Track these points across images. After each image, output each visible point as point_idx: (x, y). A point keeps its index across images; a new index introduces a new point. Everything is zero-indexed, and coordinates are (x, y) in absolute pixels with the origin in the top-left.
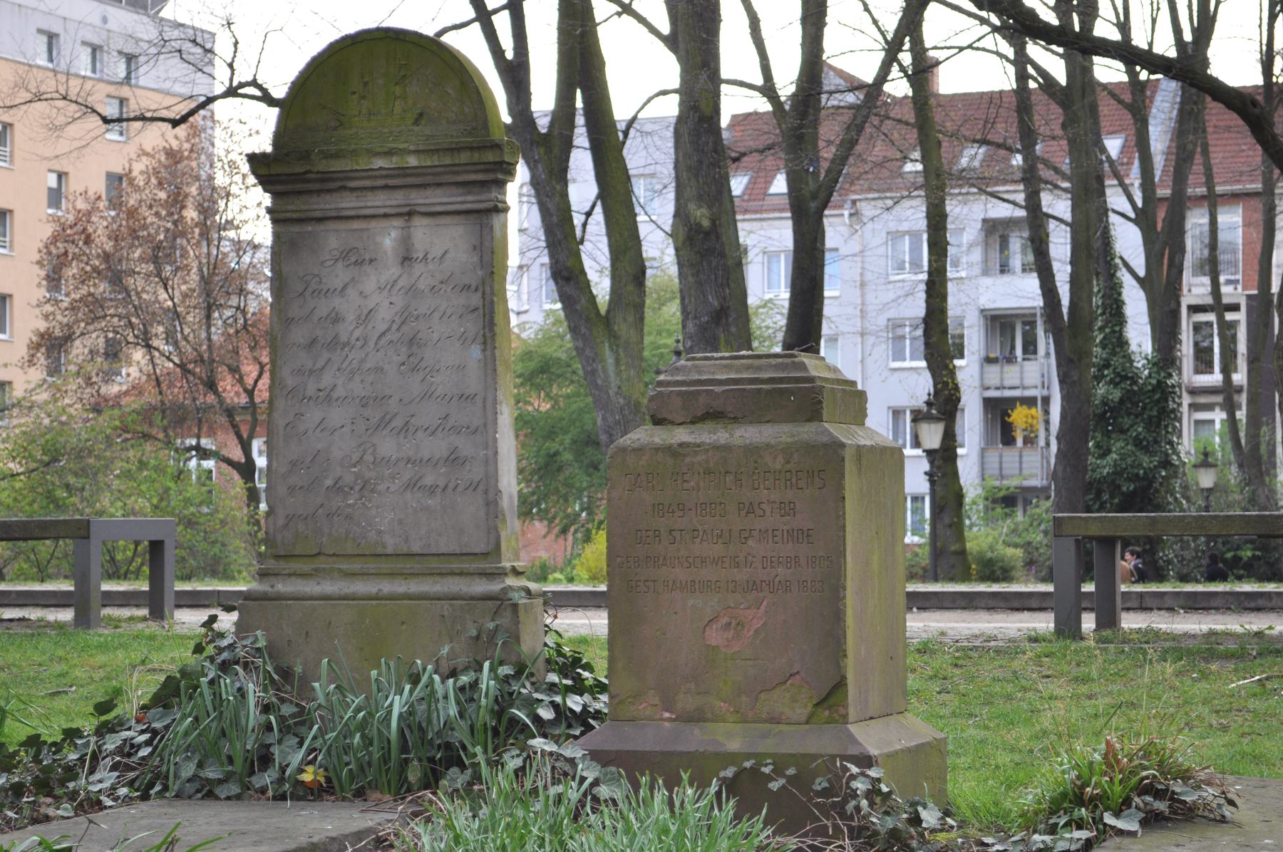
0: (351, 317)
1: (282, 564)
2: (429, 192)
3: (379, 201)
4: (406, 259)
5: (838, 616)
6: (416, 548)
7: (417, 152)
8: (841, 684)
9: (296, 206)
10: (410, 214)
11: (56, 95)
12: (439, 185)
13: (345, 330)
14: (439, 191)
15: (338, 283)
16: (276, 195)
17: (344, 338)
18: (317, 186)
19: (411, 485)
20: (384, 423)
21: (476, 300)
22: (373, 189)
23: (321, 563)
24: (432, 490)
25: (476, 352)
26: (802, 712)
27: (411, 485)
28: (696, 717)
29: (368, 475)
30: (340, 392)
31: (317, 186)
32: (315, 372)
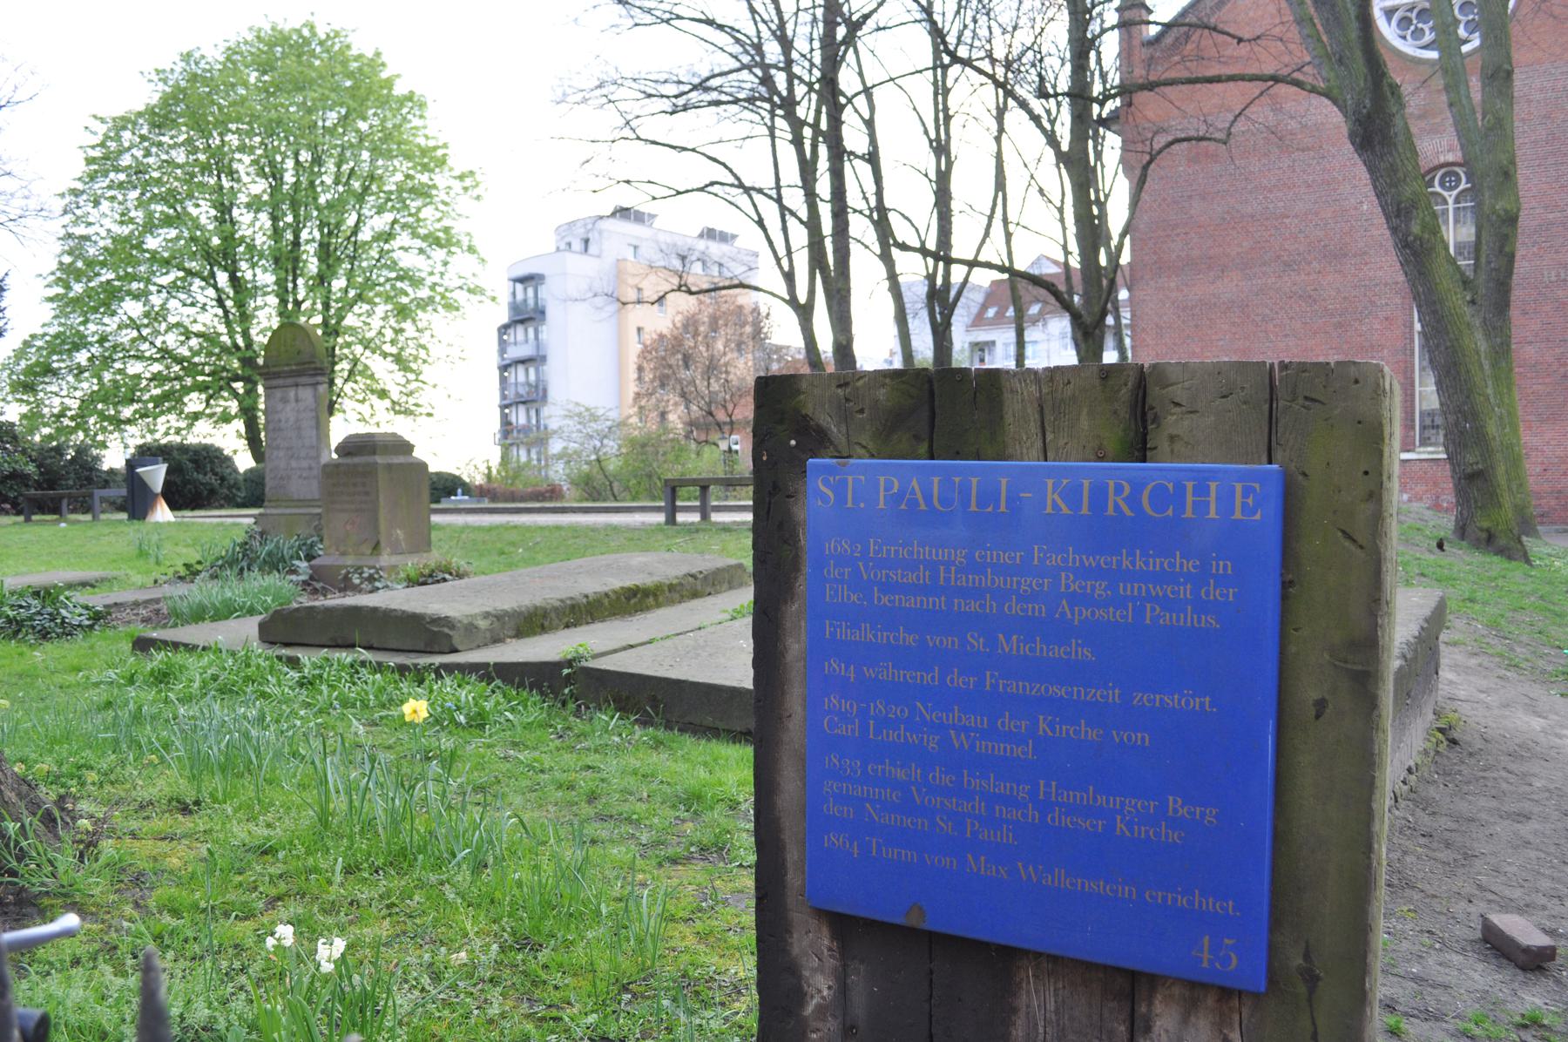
3: (290, 381)
5: (377, 520)
13: (283, 425)
28: (343, 554)
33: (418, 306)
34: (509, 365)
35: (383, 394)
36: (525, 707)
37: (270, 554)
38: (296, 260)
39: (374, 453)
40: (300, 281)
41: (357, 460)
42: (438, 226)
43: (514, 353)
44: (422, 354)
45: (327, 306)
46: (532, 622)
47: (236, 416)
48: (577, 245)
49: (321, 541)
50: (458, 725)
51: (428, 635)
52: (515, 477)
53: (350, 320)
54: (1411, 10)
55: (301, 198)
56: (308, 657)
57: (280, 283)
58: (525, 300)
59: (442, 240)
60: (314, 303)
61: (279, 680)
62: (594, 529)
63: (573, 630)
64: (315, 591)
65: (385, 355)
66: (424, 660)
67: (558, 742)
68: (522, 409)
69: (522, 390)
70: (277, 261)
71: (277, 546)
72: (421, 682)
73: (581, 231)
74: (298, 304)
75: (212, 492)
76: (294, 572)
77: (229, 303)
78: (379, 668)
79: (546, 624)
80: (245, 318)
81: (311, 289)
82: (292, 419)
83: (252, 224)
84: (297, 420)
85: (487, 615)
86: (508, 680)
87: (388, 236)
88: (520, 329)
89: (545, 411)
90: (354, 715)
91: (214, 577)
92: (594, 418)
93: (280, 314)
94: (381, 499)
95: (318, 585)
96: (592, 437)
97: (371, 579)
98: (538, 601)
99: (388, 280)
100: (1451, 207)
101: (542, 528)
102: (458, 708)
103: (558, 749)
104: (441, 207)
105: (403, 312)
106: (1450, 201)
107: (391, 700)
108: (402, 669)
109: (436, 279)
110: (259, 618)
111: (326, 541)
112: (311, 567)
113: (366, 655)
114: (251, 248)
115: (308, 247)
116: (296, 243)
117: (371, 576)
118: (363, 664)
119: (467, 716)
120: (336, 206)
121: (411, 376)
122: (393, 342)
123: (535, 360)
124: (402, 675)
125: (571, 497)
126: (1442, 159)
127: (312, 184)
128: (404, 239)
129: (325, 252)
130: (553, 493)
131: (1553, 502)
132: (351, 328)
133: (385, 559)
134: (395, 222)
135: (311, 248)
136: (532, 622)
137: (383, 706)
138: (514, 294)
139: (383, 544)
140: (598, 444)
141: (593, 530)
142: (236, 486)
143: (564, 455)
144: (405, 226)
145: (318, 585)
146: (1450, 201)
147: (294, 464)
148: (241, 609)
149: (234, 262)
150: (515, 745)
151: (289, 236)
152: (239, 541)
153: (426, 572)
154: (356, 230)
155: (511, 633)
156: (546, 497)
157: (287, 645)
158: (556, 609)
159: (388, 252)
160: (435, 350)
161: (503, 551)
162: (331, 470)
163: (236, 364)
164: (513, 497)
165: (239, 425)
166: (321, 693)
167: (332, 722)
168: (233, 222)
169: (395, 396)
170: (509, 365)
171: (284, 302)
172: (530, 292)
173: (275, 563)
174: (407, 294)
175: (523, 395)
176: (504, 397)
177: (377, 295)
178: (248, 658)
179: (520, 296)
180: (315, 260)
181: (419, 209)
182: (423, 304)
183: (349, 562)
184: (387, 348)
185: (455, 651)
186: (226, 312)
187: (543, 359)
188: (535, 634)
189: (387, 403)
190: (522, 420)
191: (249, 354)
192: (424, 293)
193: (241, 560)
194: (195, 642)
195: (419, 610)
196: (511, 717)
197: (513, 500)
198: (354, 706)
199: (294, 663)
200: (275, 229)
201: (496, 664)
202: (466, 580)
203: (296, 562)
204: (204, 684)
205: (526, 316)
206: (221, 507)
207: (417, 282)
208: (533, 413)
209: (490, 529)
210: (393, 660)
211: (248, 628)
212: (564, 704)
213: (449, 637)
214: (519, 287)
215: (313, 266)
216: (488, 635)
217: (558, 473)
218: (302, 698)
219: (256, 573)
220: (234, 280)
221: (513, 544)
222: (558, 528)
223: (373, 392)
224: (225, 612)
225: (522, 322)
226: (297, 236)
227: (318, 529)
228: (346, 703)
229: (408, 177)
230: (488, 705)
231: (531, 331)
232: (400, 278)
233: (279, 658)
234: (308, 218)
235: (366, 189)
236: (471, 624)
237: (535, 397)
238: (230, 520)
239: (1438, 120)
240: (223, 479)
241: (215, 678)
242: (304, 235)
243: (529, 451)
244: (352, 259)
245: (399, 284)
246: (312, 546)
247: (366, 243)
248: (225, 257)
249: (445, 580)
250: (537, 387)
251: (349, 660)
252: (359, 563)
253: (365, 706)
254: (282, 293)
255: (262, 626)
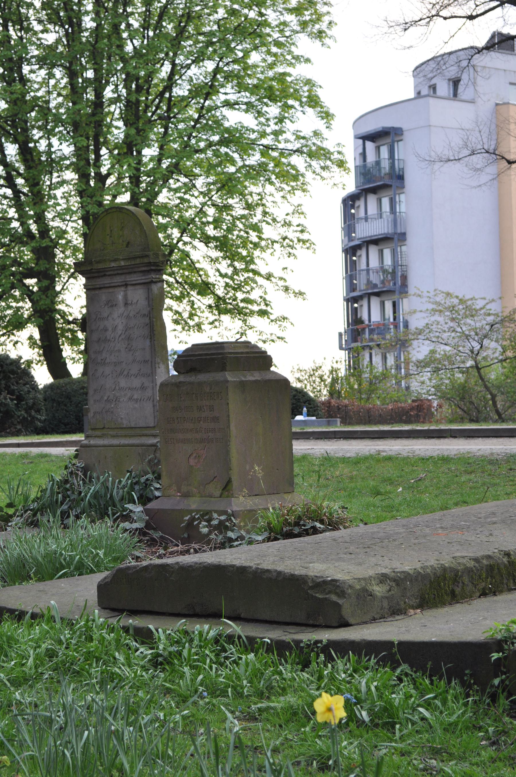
0: (110, 329)
1: (94, 432)
2: (132, 275)
3: (118, 280)
4: (126, 304)
5: (228, 453)
6: (133, 426)
7: (123, 259)
8: (229, 482)
9: (100, 282)
10: (126, 285)
11: (483, 151)
12: (135, 272)
13: (109, 334)
14: (135, 275)
15: (105, 315)
16: (87, 279)
17: (108, 338)
18: (96, 275)
19: (130, 399)
20: (121, 373)
21: (147, 320)
22: (115, 275)
23: (105, 432)
24: (136, 400)
25: (148, 342)
26: (218, 493)
27: (130, 399)
28: (186, 495)
29: (118, 395)
30: (108, 361)
31: (96, 275)
32: (100, 352)
33: (248, 176)
34: (359, 247)
35: (205, 288)
36: (444, 702)
37: (96, 495)
38: (99, 124)
39: (223, 368)
40: (104, 151)
41: (202, 377)
42: (271, 74)
43: (365, 230)
44: (253, 236)
45: (135, 180)
46: (440, 589)
47: (29, 320)
48: (444, 88)
49: (158, 478)
50: (360, 723)
51: (311, 602)
52: (371, 391)
53: (163, 197)
55: (104, 47)
56: (163, 630)
57: (80, 152)
58: (378, 163)
59: (277, 91)
60: (120, 178)
61: (128, 658)
62: (492, 461)
63: (491, 599)
64: (152, 542)
65: (207, 240)
66: (307, 636)
67: (491, 751)
68: (375, 302)
69: (375, 279)
70: (76, 126)
71: (104, 485)
72: (306, 665)
73: (452, 72)
74: (101, 179)
75: (8, 414)
76: (127, 517)
77: (20, 181)
78: (251, 645)
79: (458, 590)
80: (38, 198)
81: (117, 160)
82: (120, 327)
83: (45, 83)
84: (127, 328)
85: (383, 578)
86: (418, 665)
87: (207, 90)
88: (372, 199)
89: (405, 305)
90: (226, 705)
91: (34, 524)
92: (472, 312)
93: (81, 193)
94: (233, 427)
95: (156, 535)
96: (467, 337)
97: (222, 527)
98: (446, 561)
99: (210, 144)
101: (424, 460)
102: (359, 701)
103: (493, 760)
104: (274, 49)
105: (228, 185)
107: (270, 688)
108: (281, 648)
109: (267, 141)
110: (99, 577)
111: (164, 480)
112: (147, 512)
113: (234, 628)
114: (45, 111)
115: (112, 108)
116: (98, 103)
117: (221, 522)
118: (230, 639)
119: (370, 712)
120: (146, 57)
121: (239, 265)
122: (217, 223)
123: (393, 239)
124: (281, 655)
125: (443, 417)
127: (116, 28)
128: (228, 92)
129: (133, 114)
130: (419, 411)
132: (165, 206)
133: (240, 502)
134: (217, 70)
135: (116, 109)
136: (440, 589)
137: (261, 695)
138: (364, 155)
139: (235, 483)
140: (477, 346)
141: (491, 462)
142: (34, 407)
143: (430, 362)
144: (229, 76)
145: (156, 535)
147: (123, 383)
148: (68, 565)
149: (25, 130)
150: (436, 753)
151: (90, 95)
152: (58, 478)
153: (292, 519)
154: (170, 82)
155: (414, 602)
156: (411, 417)
157: (133, 613)
158: (469, 571)
159: (210, 109)
160: (269, 232)
161: (388, 490)
162: (169, 388)
163: (28, 255)
164: (369, 417)
165: (32, 331)
166: (182, 676)
167: (201, 714)
168: (23, 80)
169: (220, 292)
170: (359, 247)
171: (84, 177)
172: (384, 152)
173: (103, 508)
174: (233, 162)
175: (375, 282)
176: (351, 287)
177: (197, 164)
178: (89, 629)
179: (371, 158)
180: (120, 124)
181: (247, 53)
182: (256, 173)
183: (194, 507)
184: (210, 231)
185: (345, 624)
186: (17, 193)
187: (402, 237)
188: (443, 604)
189: (209, 300)
190: (376, 317)
191: (45, 243)
192: (254, 159)
193: (62, 502)
194: (23, 607)
195: (298, 571)
196: (427, 714)
197: (369, 421)
198: (224, 693)
199: (145, 636)
200: (72, 84)
201: (401, 644)
202: (342, 533)
203: (130, 506)
204: (39, 662)
205: (378, 183)
206: (17, 434)
207: (245, 146)
208: (389, 306)
209: (357, 461)
210: (269, 635)
211: (86, 589)
212: (494, 698)
213: (338, 606)
214: (370, 145)
215: (118, 131)
216: (385, 604)
217: (422, 385)
218: (159, 682)
219: (84, 520)
220: (27, 153)
221: (390, 481)
222: (445, 460)
223: (193, 286)
224: (51, 569)
225: (374, 190)
226: (99, 95)
227: (154, 464)
228: (216, 691)
229: (233, 13)
230: (397, 698)
231: (386, 202)
232: (223, 142)
233: (126, 629)
234: (111, 72)
235: (181, 32)
236: (364, 590)
237: (394, 286)
238: (35, 450)
240: (20, 399)
241: (51, 654)
242: (108, 93)
243: (385, 358)
244: (166, 120)
245: (223, 150)
246: (147, 484)
247: (183, 98)
248: (14, 126)
249: (315, 531)
250: (394, 273)
251: (212, 633)
252: (206, 507)
253: (239, 695)
254: (83, 164)
255: (102, 588)
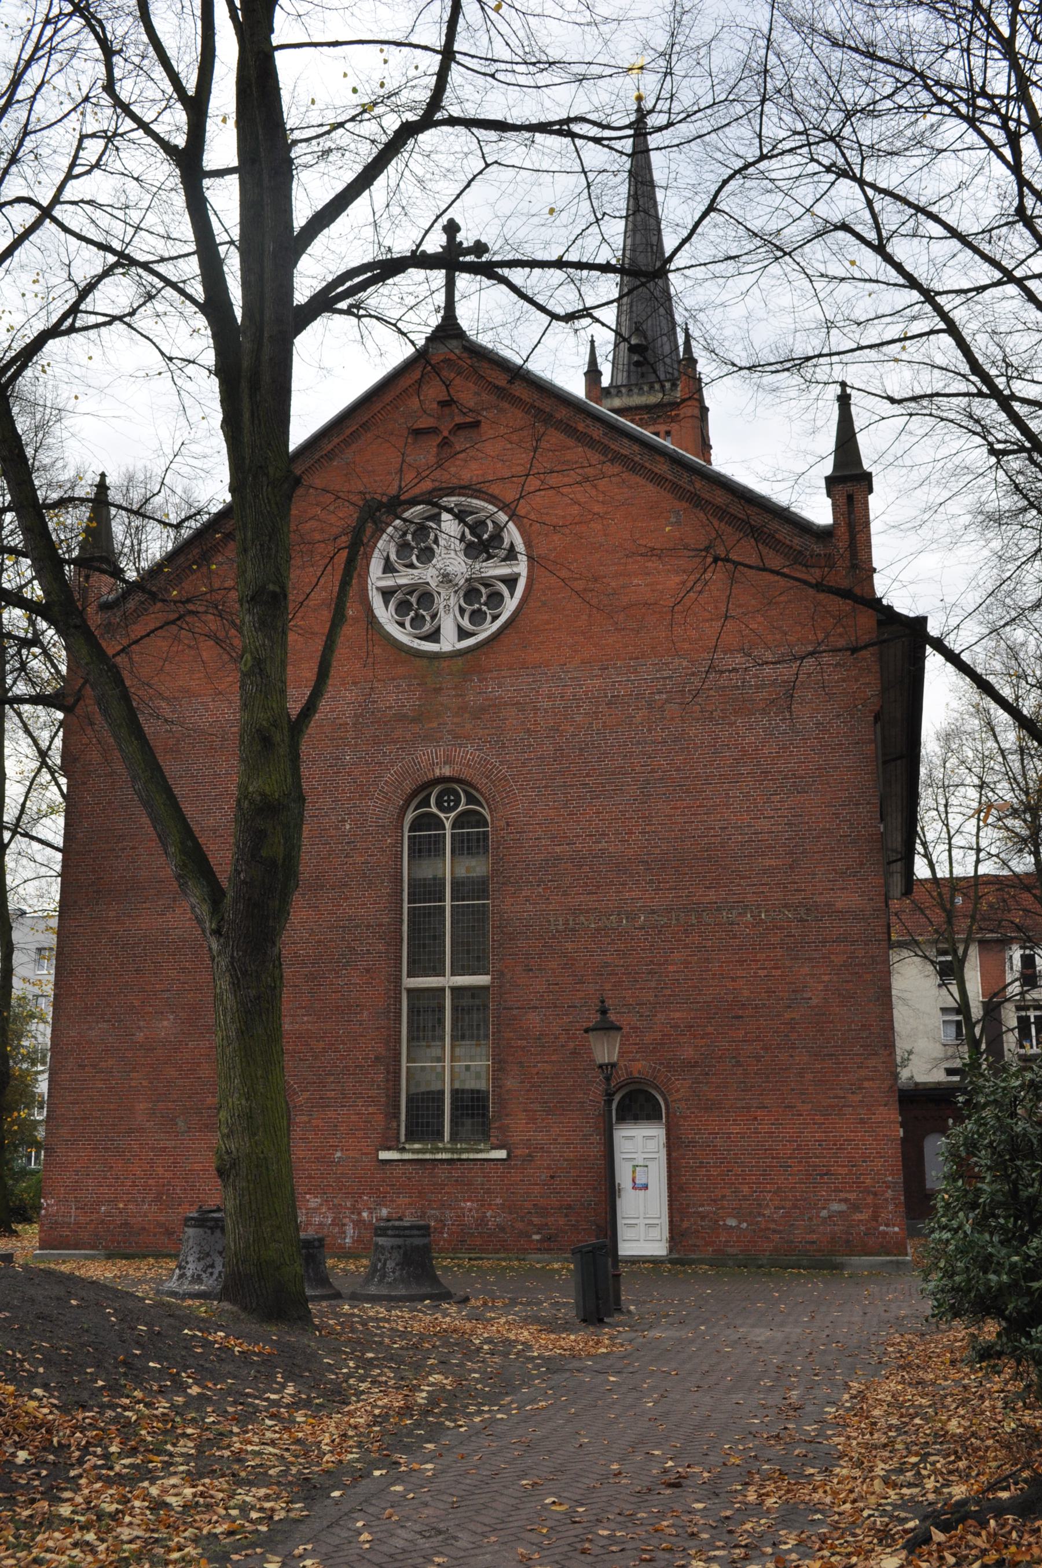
54: (411, 593)
100: (448, 833)
106: (448, 825)
126: (437, 772)
131: (562, 1221)
146: (448, 825)
239: (435, 725)
